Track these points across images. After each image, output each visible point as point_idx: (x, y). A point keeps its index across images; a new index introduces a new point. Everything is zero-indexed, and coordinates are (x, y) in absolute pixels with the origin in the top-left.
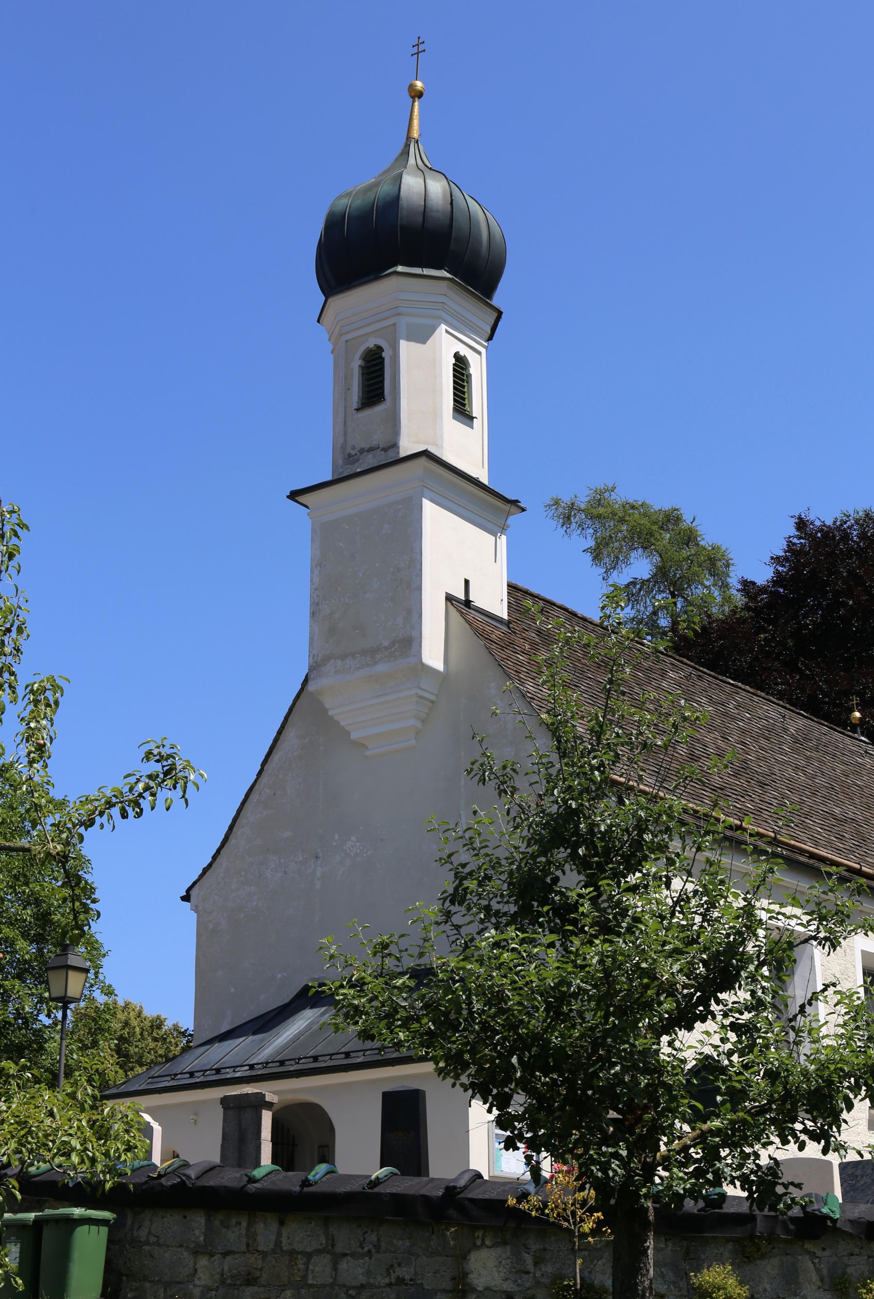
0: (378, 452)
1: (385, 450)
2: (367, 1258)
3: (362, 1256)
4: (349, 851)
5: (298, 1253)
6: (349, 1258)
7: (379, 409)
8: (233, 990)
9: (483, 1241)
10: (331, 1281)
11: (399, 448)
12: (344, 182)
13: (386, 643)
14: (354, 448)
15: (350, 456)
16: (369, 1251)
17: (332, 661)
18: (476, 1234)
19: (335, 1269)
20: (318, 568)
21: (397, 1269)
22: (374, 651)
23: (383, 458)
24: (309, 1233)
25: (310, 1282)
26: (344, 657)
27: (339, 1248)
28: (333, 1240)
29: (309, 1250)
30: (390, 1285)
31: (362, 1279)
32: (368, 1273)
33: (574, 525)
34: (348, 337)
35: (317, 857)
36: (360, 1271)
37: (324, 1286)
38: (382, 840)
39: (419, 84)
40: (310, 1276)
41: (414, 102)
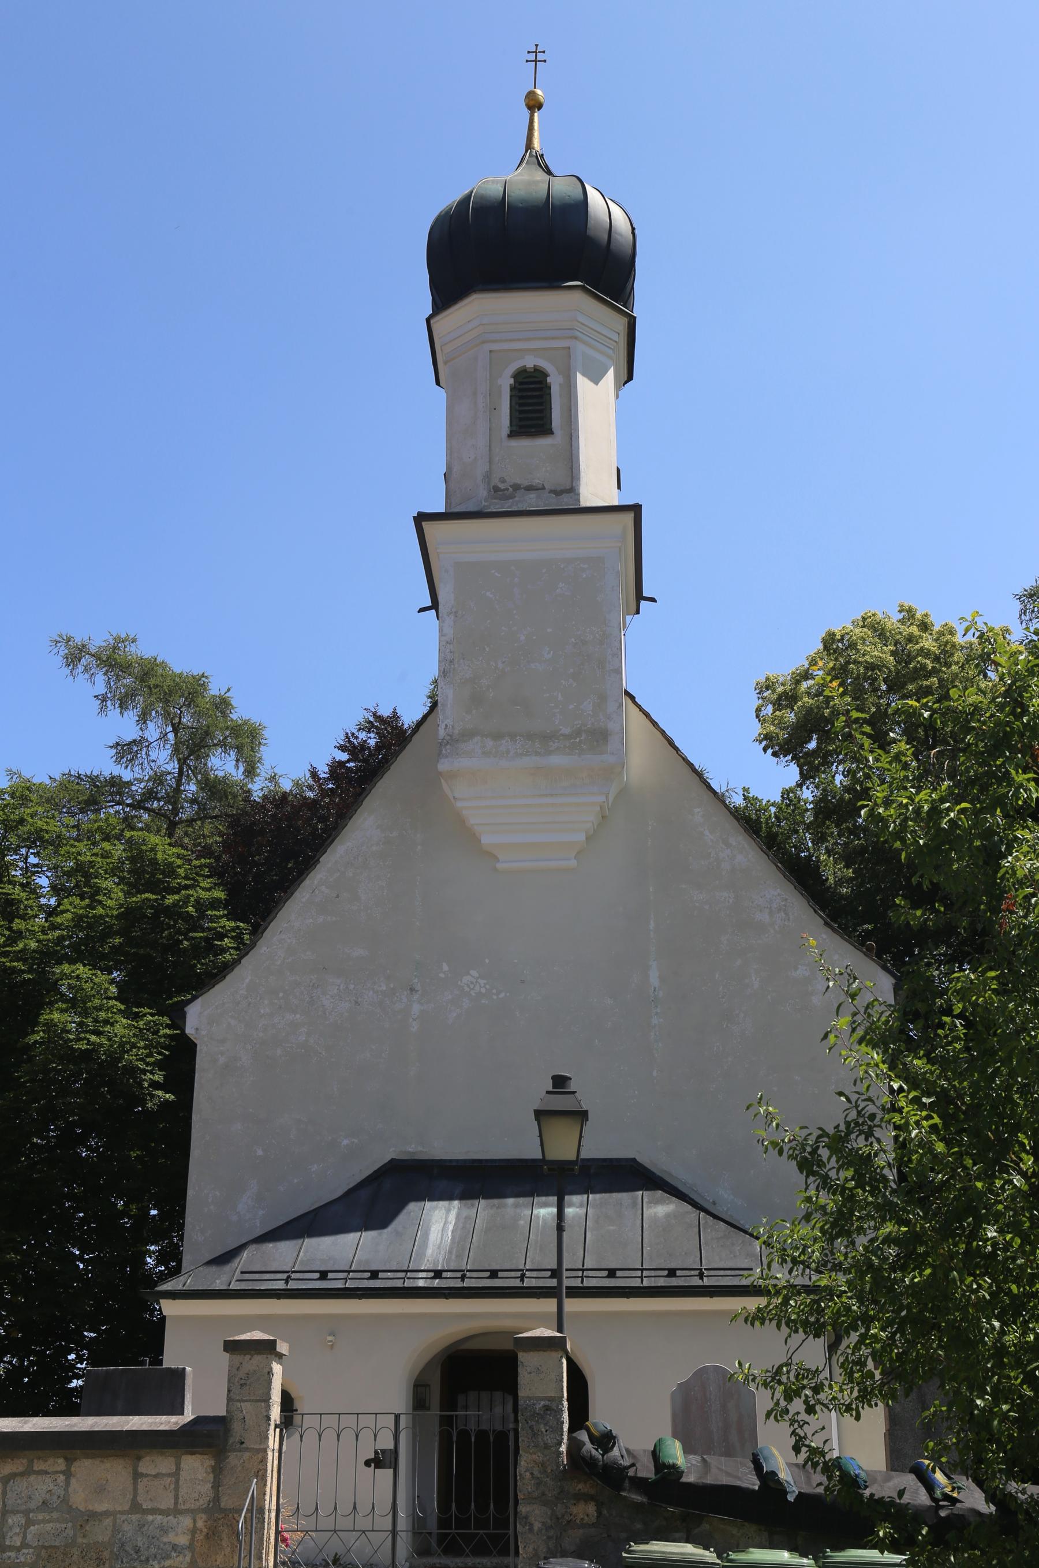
1: (558, 493)
4: (467, 989)
8: (260, 1152)
11: (579, 495)
13: (567, 731)
14: (503, 481)
15: (496, 489)
17: (477, 739)
20: (452, 617)
23: (553, 503)
26: (497, 736)
33: (81, 668)
34: (495, 347)
35: (412, 990)
38: (523, 982)
39: (539, 92)
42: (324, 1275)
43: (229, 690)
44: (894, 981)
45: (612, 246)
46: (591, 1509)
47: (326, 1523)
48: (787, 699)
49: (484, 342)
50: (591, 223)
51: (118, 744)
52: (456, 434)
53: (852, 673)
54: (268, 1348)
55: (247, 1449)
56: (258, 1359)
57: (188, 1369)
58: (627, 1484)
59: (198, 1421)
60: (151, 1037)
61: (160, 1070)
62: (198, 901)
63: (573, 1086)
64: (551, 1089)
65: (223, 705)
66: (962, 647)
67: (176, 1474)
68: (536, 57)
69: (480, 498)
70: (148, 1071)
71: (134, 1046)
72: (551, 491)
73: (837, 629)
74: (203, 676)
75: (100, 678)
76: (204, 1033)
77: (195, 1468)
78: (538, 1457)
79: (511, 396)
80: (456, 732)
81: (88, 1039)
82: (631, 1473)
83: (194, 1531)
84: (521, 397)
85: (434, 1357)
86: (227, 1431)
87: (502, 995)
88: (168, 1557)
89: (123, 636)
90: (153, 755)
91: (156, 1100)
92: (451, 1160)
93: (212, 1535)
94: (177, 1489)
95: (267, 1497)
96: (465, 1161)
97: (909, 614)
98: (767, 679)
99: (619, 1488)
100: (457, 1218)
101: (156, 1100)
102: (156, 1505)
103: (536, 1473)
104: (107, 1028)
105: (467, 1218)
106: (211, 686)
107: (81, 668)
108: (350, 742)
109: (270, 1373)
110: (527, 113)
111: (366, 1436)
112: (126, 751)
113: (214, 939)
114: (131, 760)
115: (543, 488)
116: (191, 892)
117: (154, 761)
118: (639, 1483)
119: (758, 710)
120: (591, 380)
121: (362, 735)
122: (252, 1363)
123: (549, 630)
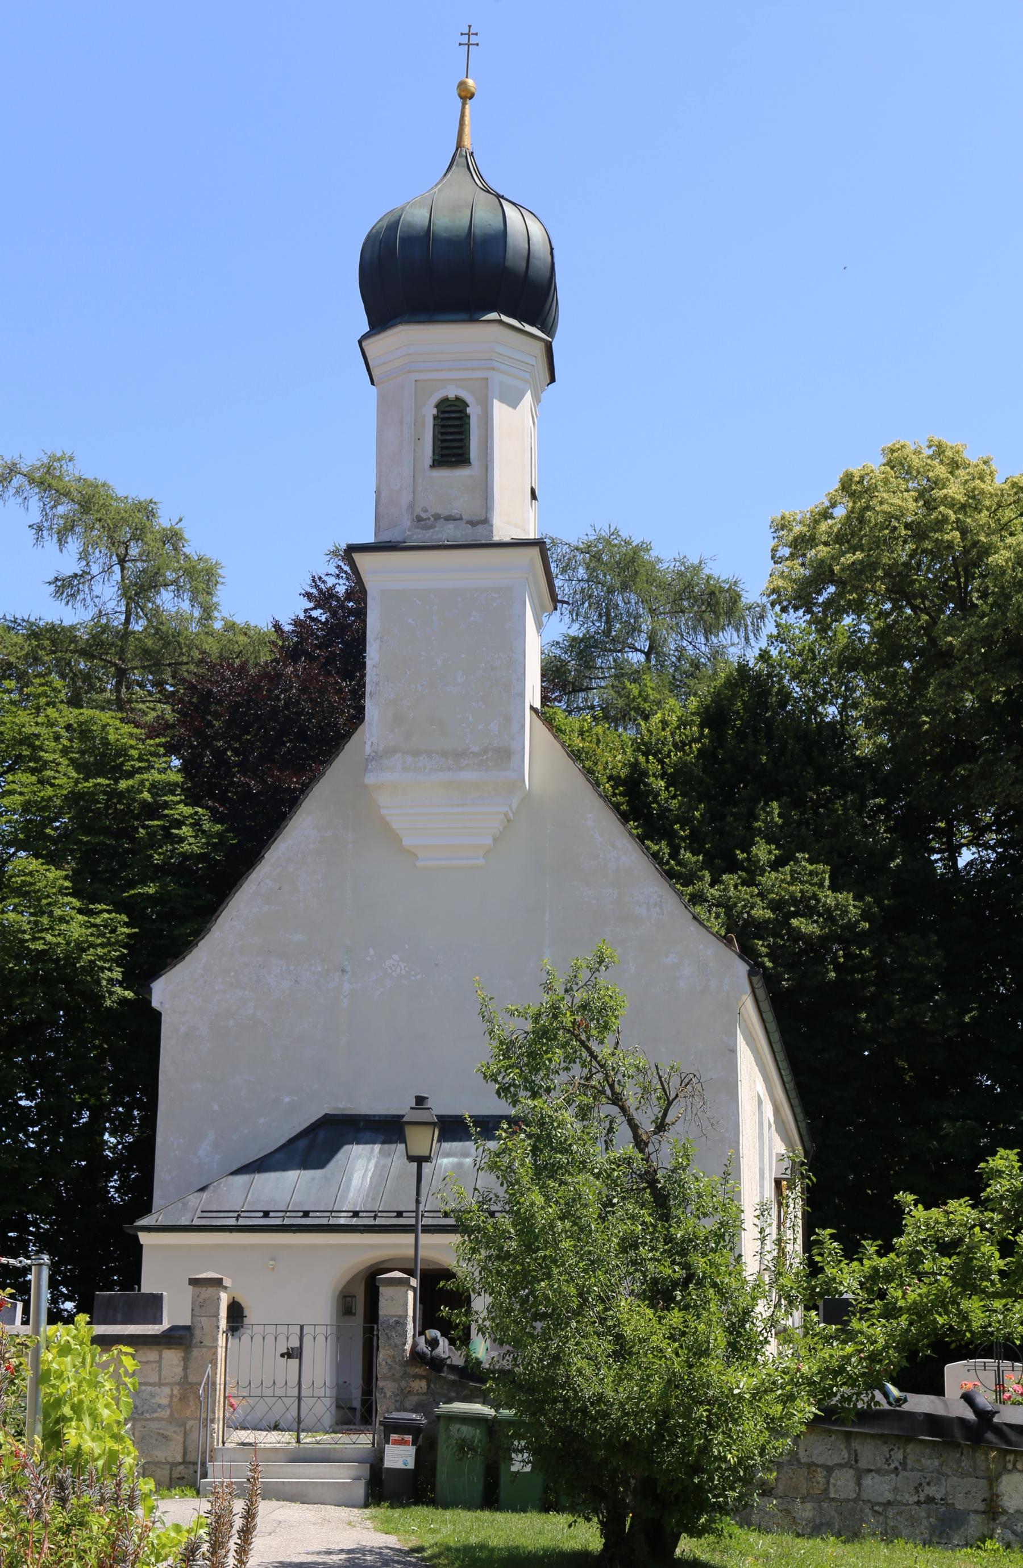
0: (462, 524)
1: (473, 523)
2: (893, 1476)
3: (888, 1472)
4: (389, 971)
5: (818, 1466)
6: (874, 1474)
7: (460, 473)
9: (1014, 1465)
10: (855, 1496)
11: (492, 526)
12: (416, 191)
13: (475, 749)
14: (425, 511)
15: (419, 519)
16: (896, 1468)
17: (399, 755)
18: (1008, 1458)
19: (859, 1484)
21: (927, 1488)
22: (459, 755)
24: (829, 1447)
25: (832, 1496)
26: (416, 753)
27: (863, 1464)
28: (856, 1455)
29: (829, 1463)
30: (918, 1503)
31: (888, 1496)
32: (895, 1490)
33: (12, 491)
34: (420, 376)
35: (343, 971)
36: (887, 1488)
37: (847, 1500)
38: (436, 965)
39: (470, 82)
40: (832, 1490)
41: (464, 104)
42: (266, 1214)
43: (181, 520)
44: (748, 968)
45: (530, 273)
46: (424, 1384)
47: (257, 1392)
48: (801, 543)
49: (409, 372)
50: (510, 252)
51: (57, 579)
52: (385, 461)
53: (869, 521)
54: (218, 1283)
55: (205, 1346)
56: (211, 1291)
57: (165, 1294)
58: (445, 1369)
59: (173, 1328)
60: (108, 935)
61: (118, 966)
62: (153, 785)
63: (429, 1104)
64: (414, 1105)
65: (173, 538)
66: (991, 495)
67: (159, 1361)
68: (469, 40)
69: (403, 529)
70: (105, 968)
71: (93, 946)
72: (469, 522)
73: (856, 470)
74: (151, 502)
75: (35, 504)
76: (167, 1006)
77: (172, 1357)
78: (391, 1352)
79: (434, 425)
80: (381, 749)
81: (44, 938)
82: (448, 1362)
83: (172, 1396)
84: (443, 426)
85: (360, 1272)
86: (192, 1335)
87: (419, 977)
88: (156, 1411)
89: (59, 454)
90: (97, 589)
91: (115, 998)
92: (374, 1116)
93: (183, 1398)
94: (160, 1371)
95: (218, 1376)
96: (386, 1116)
97: (940, 450)
98: (783, 518)
99: (440, 1371)
100: (376, 1166)
101: (115, 998)
102: (146, 1380)
103: (389, 1362)
104: (64, 926)
105: (384, 1166)
106: (160, 513)
107: (12, 491)
108: (317, 586)
109: (219, 1299)
110: (459, 102)
111: (282, 1339)
112: (66, 587)
113: (171, 827)
114: (72, 595)
115: (461, 519)
116: (145, 776)
117: (97, 597)
118: (453, 1368)
119: (774, 550)
120: (509, 405)
121: (331, 581)
122: (208, 1292)
123: (463, 656)
